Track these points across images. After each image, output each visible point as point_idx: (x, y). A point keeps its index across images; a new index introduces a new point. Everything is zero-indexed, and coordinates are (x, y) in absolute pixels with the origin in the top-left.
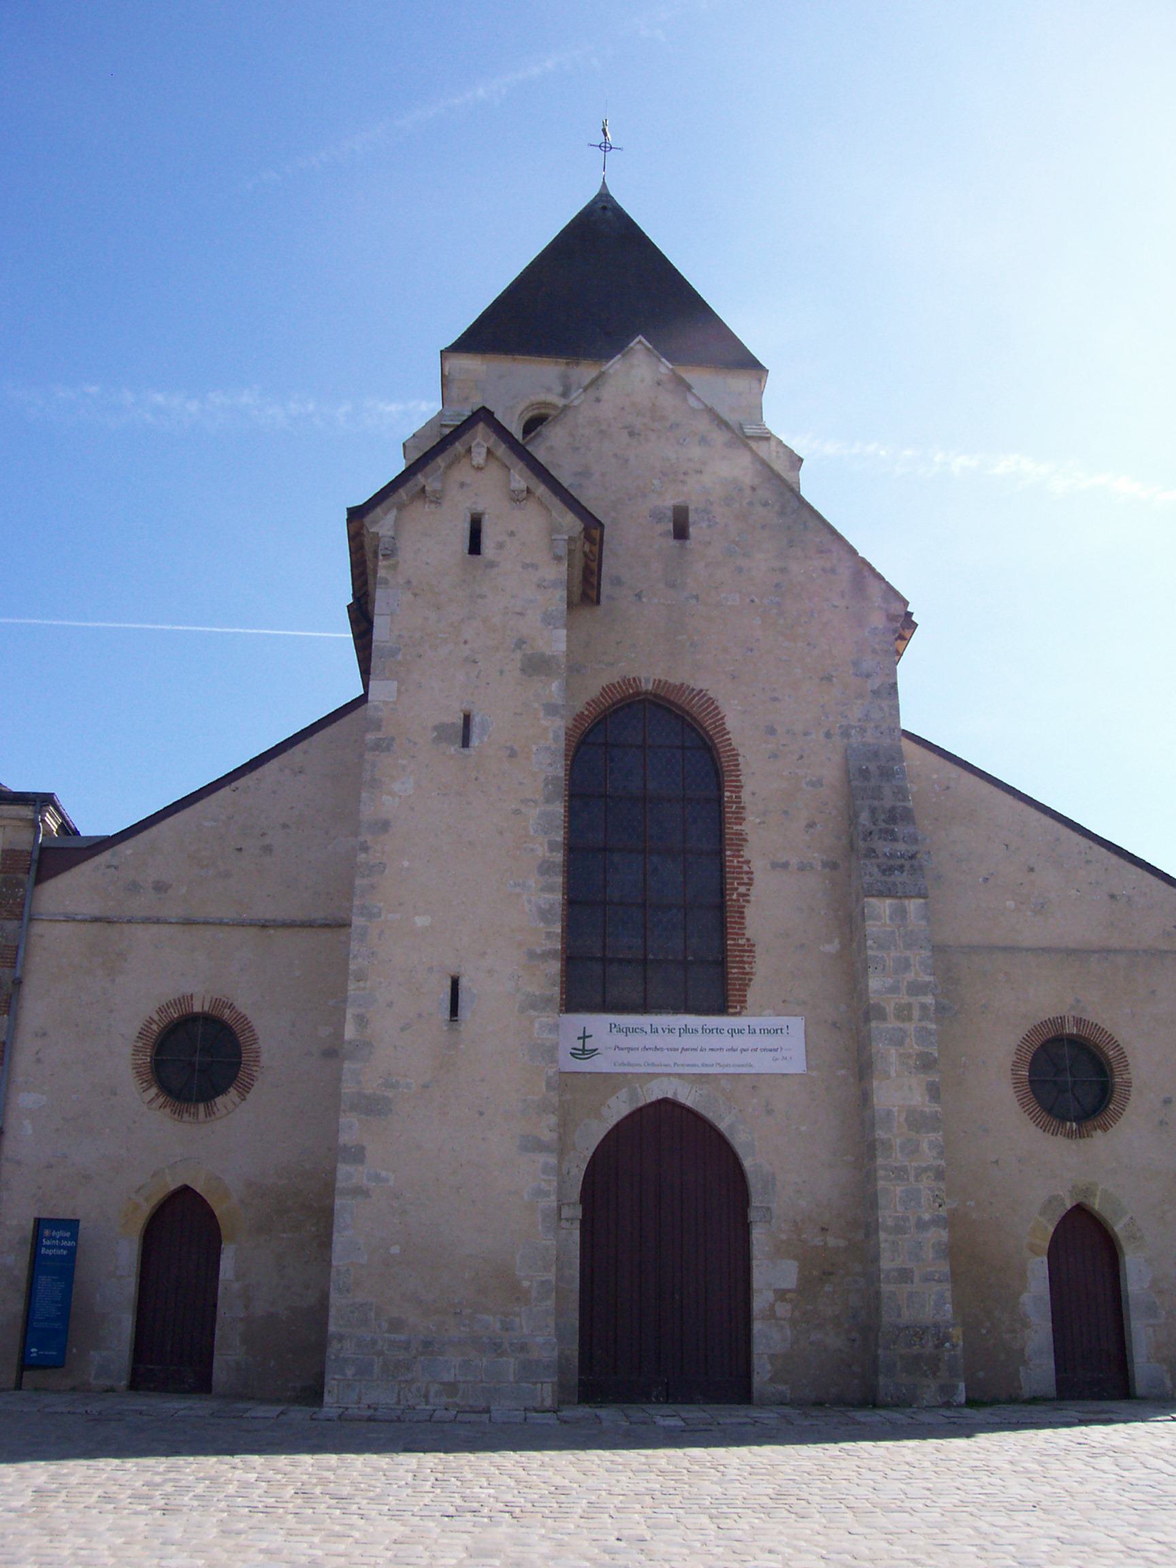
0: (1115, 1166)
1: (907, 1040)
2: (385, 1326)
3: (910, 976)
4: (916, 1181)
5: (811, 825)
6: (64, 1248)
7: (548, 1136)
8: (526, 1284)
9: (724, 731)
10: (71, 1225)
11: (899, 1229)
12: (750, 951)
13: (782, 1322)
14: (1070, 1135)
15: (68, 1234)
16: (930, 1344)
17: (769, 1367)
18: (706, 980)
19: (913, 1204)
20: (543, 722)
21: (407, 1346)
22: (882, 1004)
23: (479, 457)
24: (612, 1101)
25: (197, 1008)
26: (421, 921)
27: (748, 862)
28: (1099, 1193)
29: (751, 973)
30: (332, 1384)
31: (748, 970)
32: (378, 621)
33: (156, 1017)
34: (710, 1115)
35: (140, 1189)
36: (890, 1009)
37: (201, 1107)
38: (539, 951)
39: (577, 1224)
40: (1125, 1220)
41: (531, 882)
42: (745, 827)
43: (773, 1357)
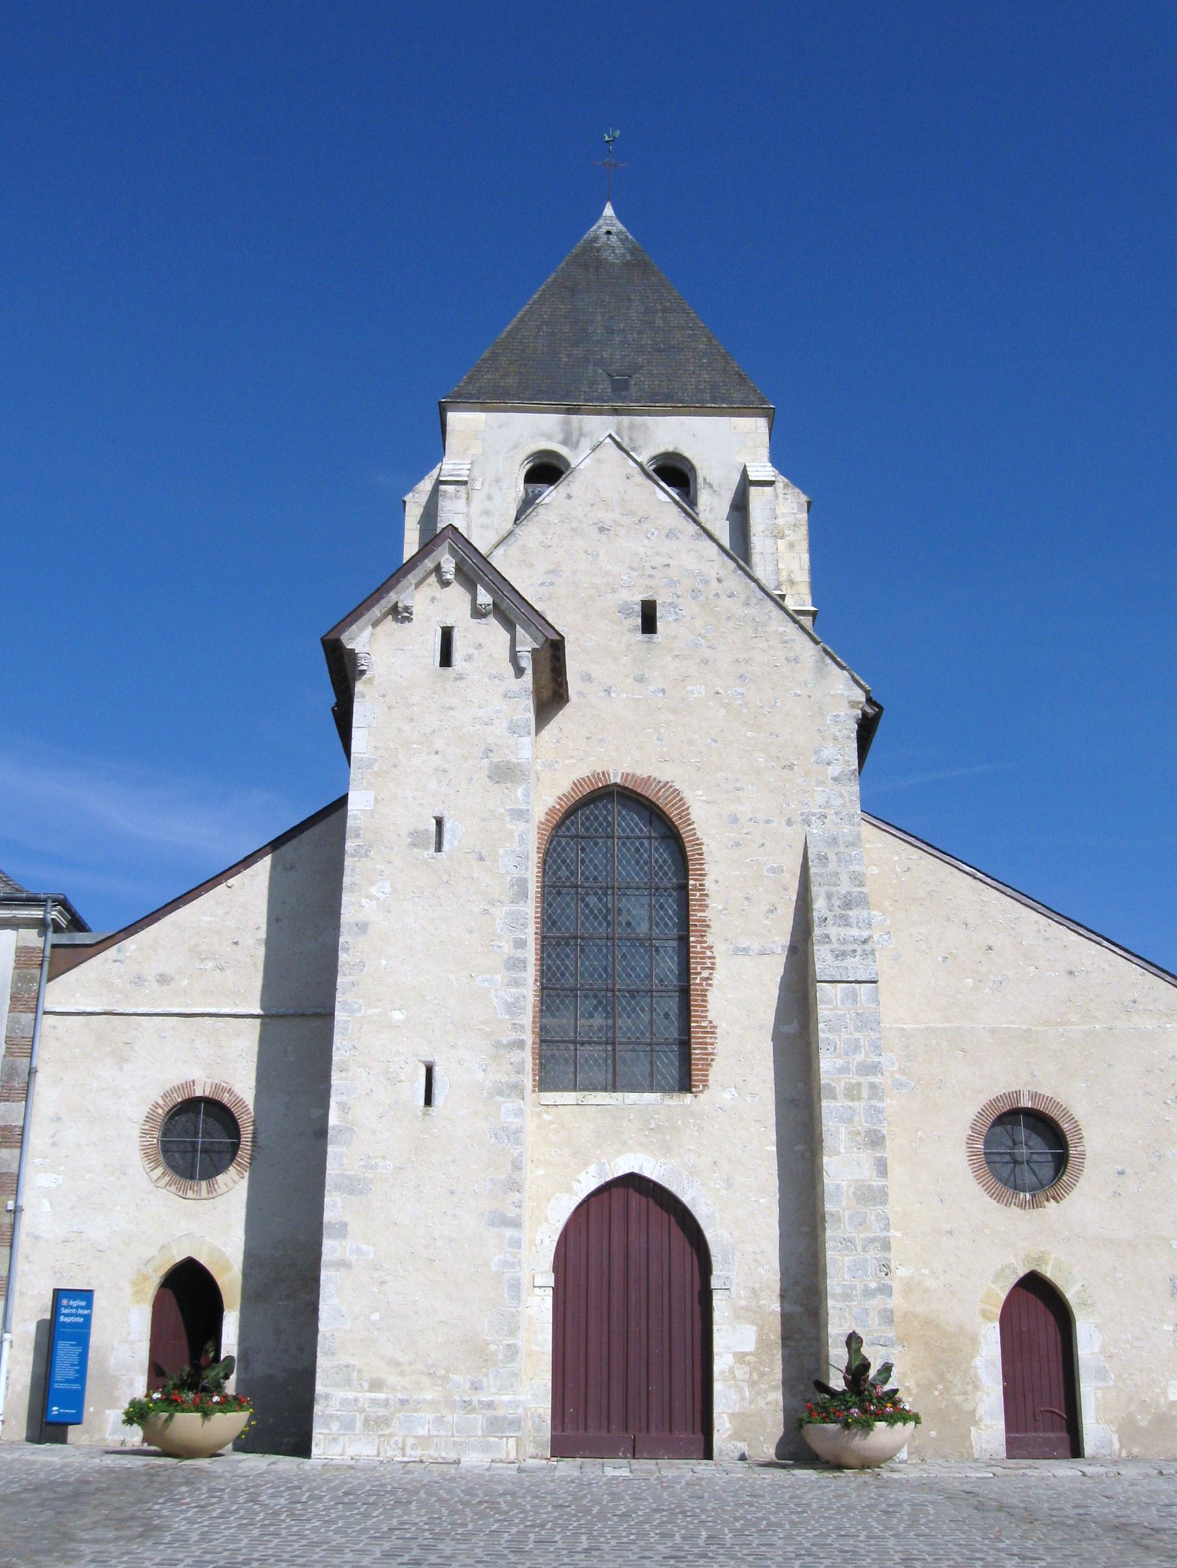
0: (1063, 1237)
1: (857, 1118)
2: (366, 1386)
3: (859, 1057)
4: (864, 1250)
5: (773, 910)
6: (81, 1315)
8: (493, 1347)
10: (86, 1295)
11: (847, 1297)
12: (713, 1033)
13: (741, 1383)
14: (1022, 1205)
15: (83, 1304)
17: (728, 1425)
18: (679, 1065)
20: (509, 826)
21: (386, 1403)
23: (449, 566)
24: (582, 1176)
25: (199, 1093)
26: (397, 1016)
27: (710, 948)
28: (1051, 1262)
29: (713, 1054)
30: (319, 1434)
31: (710, 1051)
32: (355, 733)
33: (161, 1102)
34: (673, 1188)
35: (149, 1261)
36: (840, 1088)
37: (204, 1183)
38: (505, 1042)
39: (550, 1292)
41: (498, 977)
43: (732, 1416)
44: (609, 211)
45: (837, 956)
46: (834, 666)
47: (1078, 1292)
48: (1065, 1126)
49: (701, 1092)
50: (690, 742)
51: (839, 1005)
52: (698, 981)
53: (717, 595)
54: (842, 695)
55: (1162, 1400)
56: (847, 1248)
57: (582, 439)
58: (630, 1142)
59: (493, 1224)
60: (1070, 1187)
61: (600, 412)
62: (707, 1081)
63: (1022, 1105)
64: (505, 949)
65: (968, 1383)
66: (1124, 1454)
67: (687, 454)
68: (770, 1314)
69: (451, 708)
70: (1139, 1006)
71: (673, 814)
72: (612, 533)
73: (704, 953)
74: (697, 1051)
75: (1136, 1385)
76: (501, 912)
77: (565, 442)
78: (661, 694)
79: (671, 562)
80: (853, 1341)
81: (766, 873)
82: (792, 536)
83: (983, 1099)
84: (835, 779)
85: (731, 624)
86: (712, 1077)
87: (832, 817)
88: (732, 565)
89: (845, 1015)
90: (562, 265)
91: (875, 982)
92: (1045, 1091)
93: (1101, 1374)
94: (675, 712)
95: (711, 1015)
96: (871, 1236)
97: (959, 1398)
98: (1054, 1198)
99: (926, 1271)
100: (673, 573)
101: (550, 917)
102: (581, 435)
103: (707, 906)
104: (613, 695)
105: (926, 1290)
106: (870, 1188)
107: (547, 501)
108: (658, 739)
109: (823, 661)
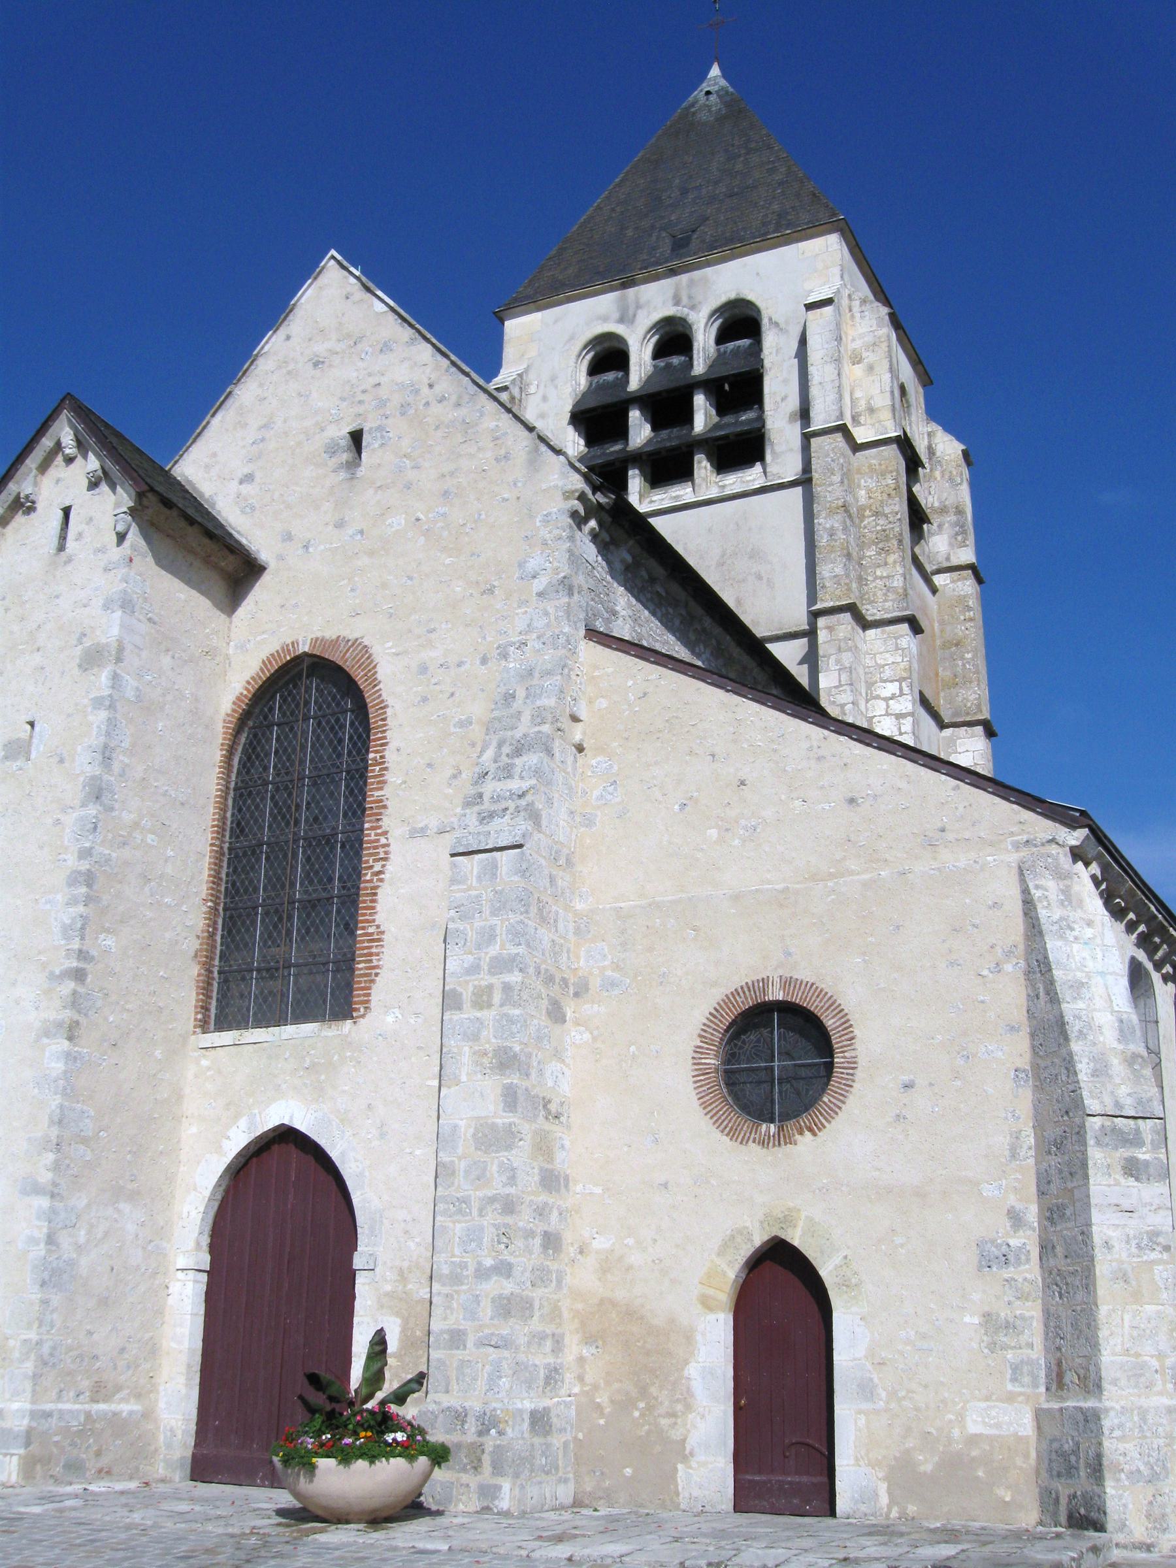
1: (484, 1033)
3: (494, 950)
4: (481, 1215)
7: (45, 1177)
9: (375, 683)
14: (763, 1143)
16: (473, 1430)
19: (473, 1245)
22: (459, 989)
24: (232, 1133)
27: (386, 833)
28: (801, 1224)
29: (377, 967)
31: (375, 963)
38: (57, 972)
40: (837, 1259)
41: (59, 897)
42: (387, 792)
44: (715, 71)
45: (484, 819)
46: (550, 453)
47: (837, 1267)
48: (829, 1023)
49: (363, 1016)
50: (384, 585)
51: (474, 884)
52: (368, 878)
53: (427, 404)
54: (556, 487)
55: (956, 1433)
56: (460, 1211)
57: (639, 311)
58: (284, 1086)
59: (25, 1192)
60: (834, 1111)
61: (657, 278)
62: (368, 1001)
63: (770, 997)
64: (70, 863)
65: (678, 1400)
66: (894, 1514)
67: (749, 298)
68: (418, 1302)
69: (57, 597)
70: (950, 836)
71: (359, 676)
72: (327, 364)
73: (378, 841)
74: (360, 966)
75: (917, 1409)
76: (70, 819)
77: (621, 320)
78: (359, 536)
79: (383, 380)
80: (379, 1343)
81: (453, 730)
82: (870, 357)
83: (716, 995)
84: (540, 594)
85: (439, 433)
86: (374, 999)
87: (533, 644)
88: (446, 362)
89: (479, 896)
90: (653, 140)
91: (520, 846)
92: (804, 974)
93: (866, 1390)
94: (371, 553)
95: (379, 918)
96: (490, 1193)
97: (664, 1422)
98: (810, 1130)
99: (630, 1241)
100: (383, 392)
101: (239, 824)
102: (638, 307)
103: (385, 782)
104: (311, 550)
105: (629, 1268)
106: (493, 1127)
107: (266, 349)
108: (352, 590)
109: (536, 450)
